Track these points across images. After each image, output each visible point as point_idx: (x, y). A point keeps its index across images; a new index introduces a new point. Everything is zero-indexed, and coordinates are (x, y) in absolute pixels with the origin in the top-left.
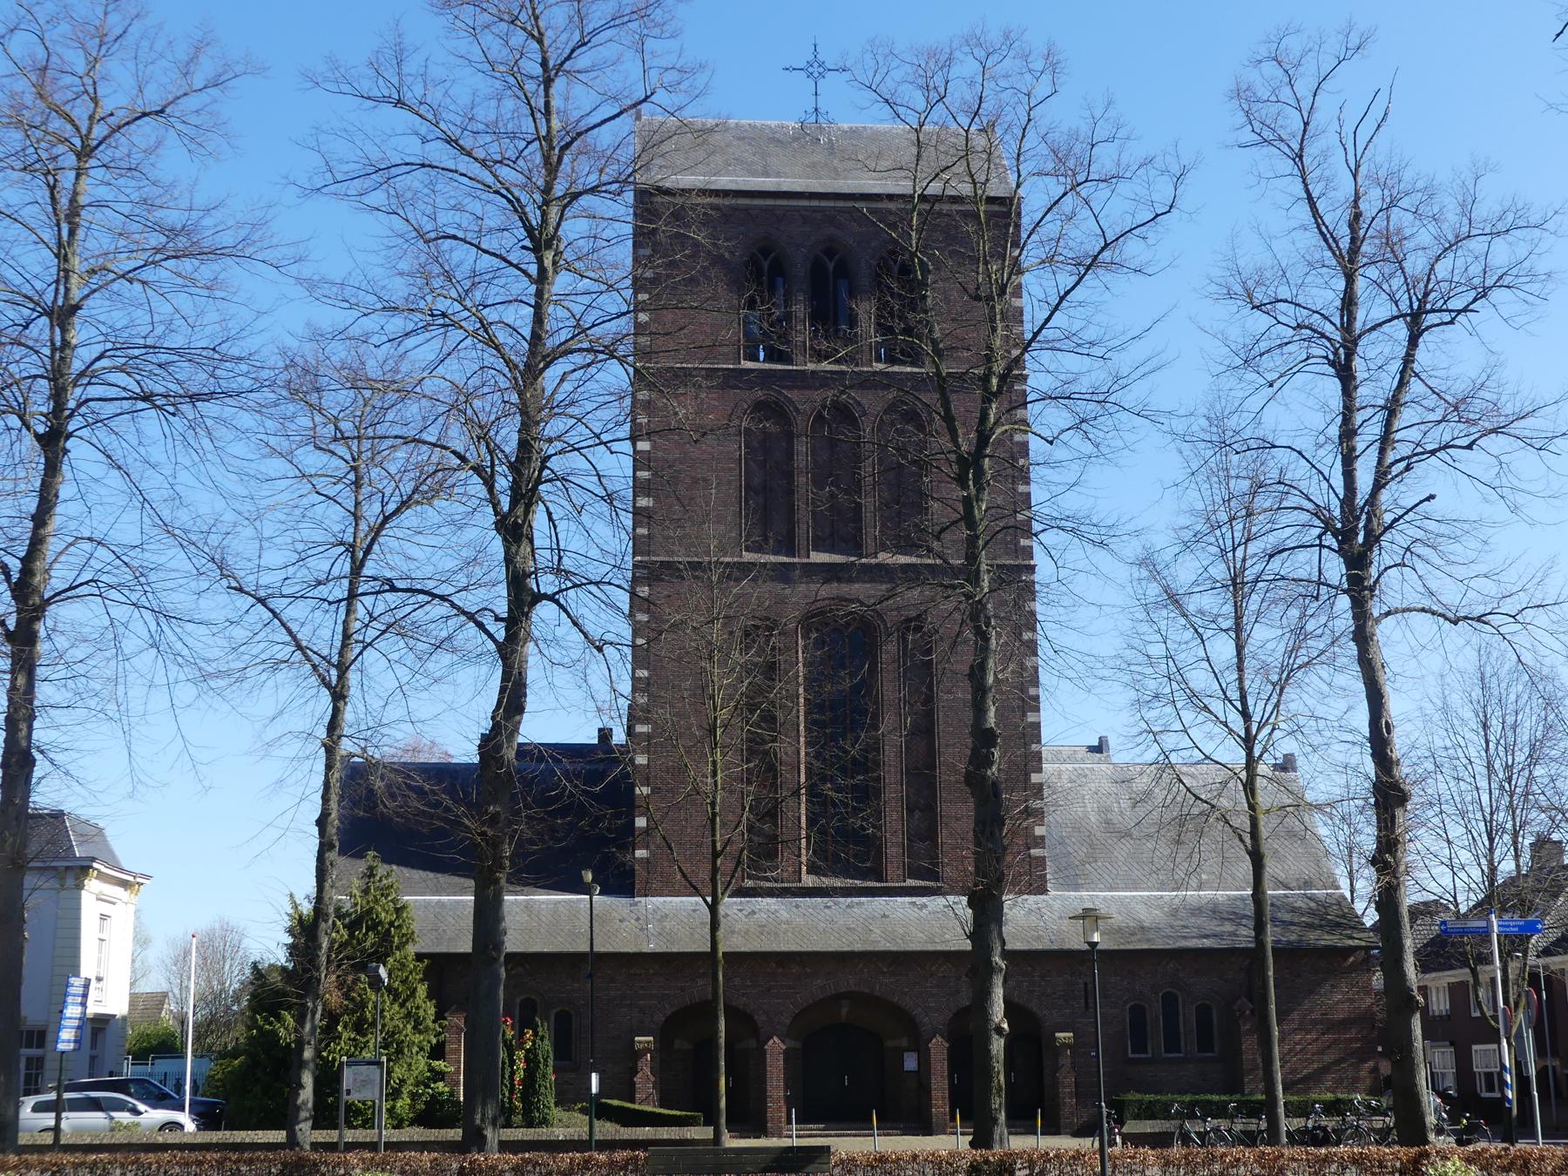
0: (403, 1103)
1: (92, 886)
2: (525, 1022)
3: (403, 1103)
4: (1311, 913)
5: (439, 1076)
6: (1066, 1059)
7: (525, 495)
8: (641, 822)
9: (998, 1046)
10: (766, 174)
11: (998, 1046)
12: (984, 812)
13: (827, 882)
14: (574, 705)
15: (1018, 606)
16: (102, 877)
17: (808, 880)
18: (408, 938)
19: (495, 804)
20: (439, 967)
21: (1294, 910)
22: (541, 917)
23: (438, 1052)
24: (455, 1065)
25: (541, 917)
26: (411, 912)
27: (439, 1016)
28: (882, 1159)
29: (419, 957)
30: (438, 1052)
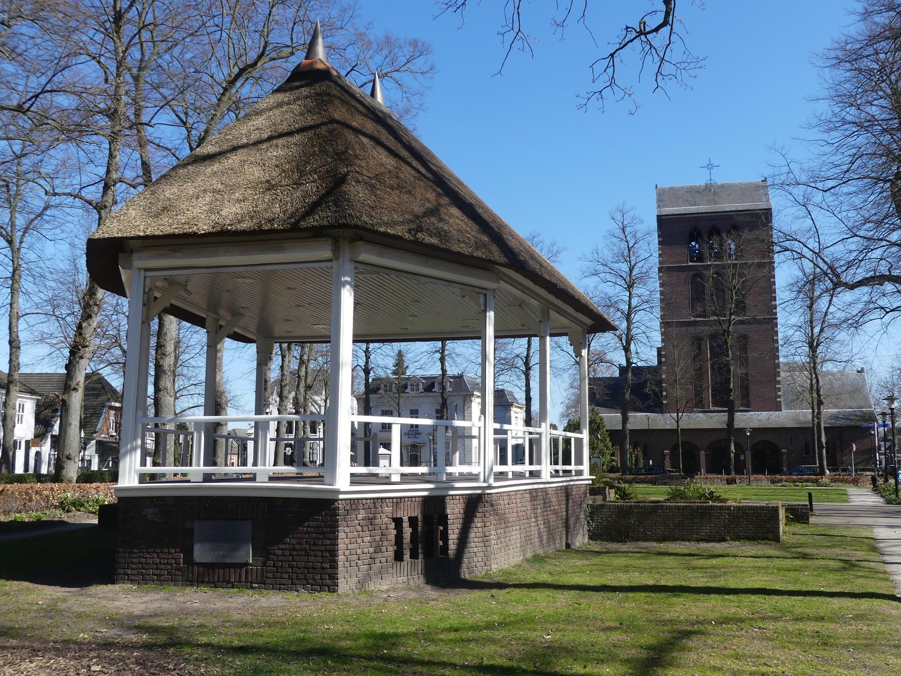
0: (605, 467)
1: (514, 409)
2: (634, 448)
3: (605, 467)
4: (861, 416)
5: (613, 461)
6: (785, 457)
7: (628, 343)
8: (664, 393)
9: (732, 455)
10: (695, 205)
11: (732, 455)
12: (762, 386)
13: (717, 409)
14: (646, 354)
15: (773, 329)
16: (516, 407)
17: (712, 408)
18: (604, 426)
19: (624, 394)
20: (613, 433)
21: (857, 416)
22: (639, 420)
23: (613, 455)
24: (617, 458)
25: (639, 420)
26: (604, 419)
27: (613, 446)
28: (417, 426)
29: (607, 431)
30: (613, 455)
